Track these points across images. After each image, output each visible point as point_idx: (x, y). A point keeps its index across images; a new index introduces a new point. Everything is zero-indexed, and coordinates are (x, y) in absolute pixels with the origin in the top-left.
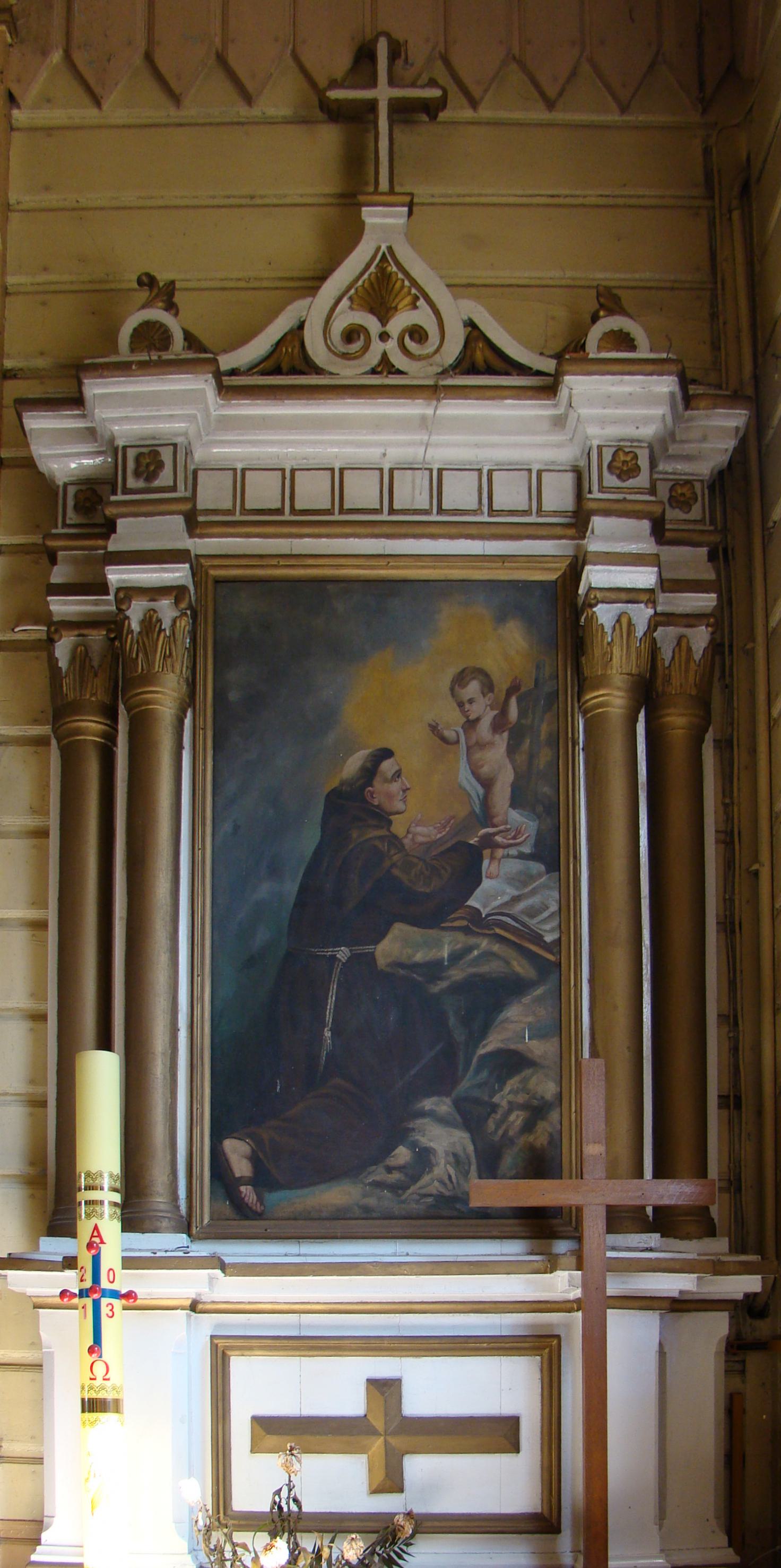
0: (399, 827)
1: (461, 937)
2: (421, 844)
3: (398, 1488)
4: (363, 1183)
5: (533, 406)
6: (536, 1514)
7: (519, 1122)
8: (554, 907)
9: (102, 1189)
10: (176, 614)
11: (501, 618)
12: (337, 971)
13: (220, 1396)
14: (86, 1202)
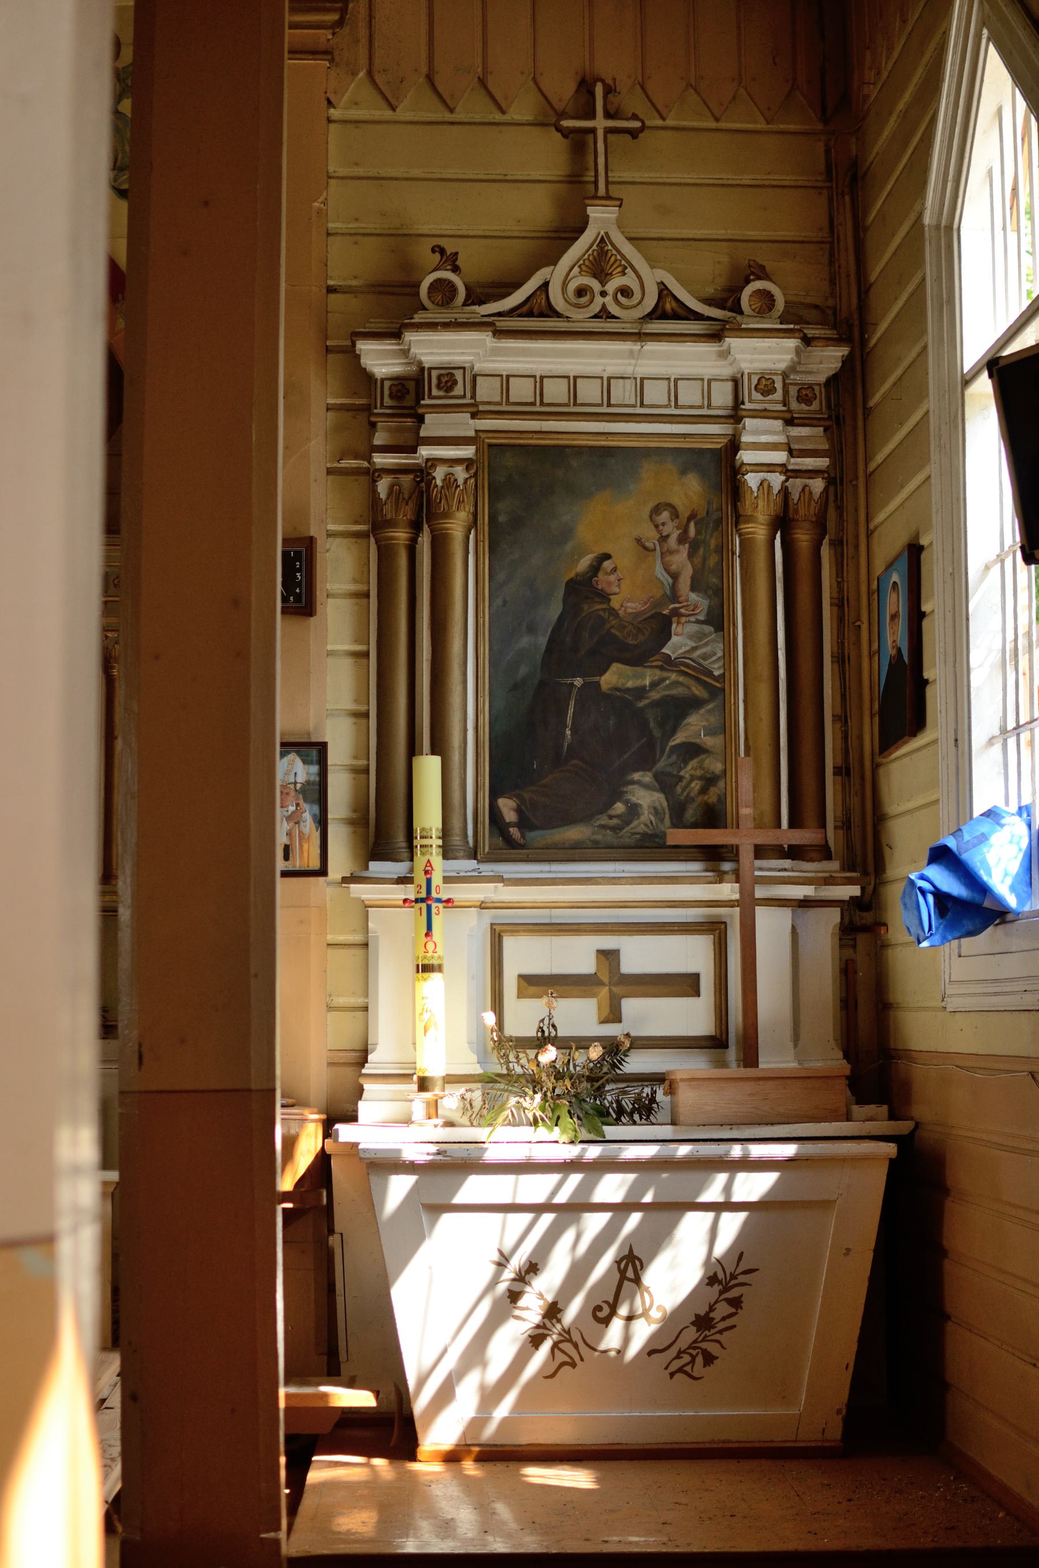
0: (615, 603)
1: (658, 672)
2: (630, 614)
3: (619, 1020)
4: (592, 826)
5: (706, 346)
6: (712, 1036)
7: (698, 787)
8: (720, 654)
9: (431, 838)
10: (467, 476)
11: (683, 472)
12: (575, 692)
13: (497, 962)
14: (421, 846)
